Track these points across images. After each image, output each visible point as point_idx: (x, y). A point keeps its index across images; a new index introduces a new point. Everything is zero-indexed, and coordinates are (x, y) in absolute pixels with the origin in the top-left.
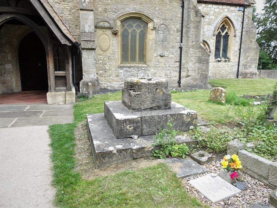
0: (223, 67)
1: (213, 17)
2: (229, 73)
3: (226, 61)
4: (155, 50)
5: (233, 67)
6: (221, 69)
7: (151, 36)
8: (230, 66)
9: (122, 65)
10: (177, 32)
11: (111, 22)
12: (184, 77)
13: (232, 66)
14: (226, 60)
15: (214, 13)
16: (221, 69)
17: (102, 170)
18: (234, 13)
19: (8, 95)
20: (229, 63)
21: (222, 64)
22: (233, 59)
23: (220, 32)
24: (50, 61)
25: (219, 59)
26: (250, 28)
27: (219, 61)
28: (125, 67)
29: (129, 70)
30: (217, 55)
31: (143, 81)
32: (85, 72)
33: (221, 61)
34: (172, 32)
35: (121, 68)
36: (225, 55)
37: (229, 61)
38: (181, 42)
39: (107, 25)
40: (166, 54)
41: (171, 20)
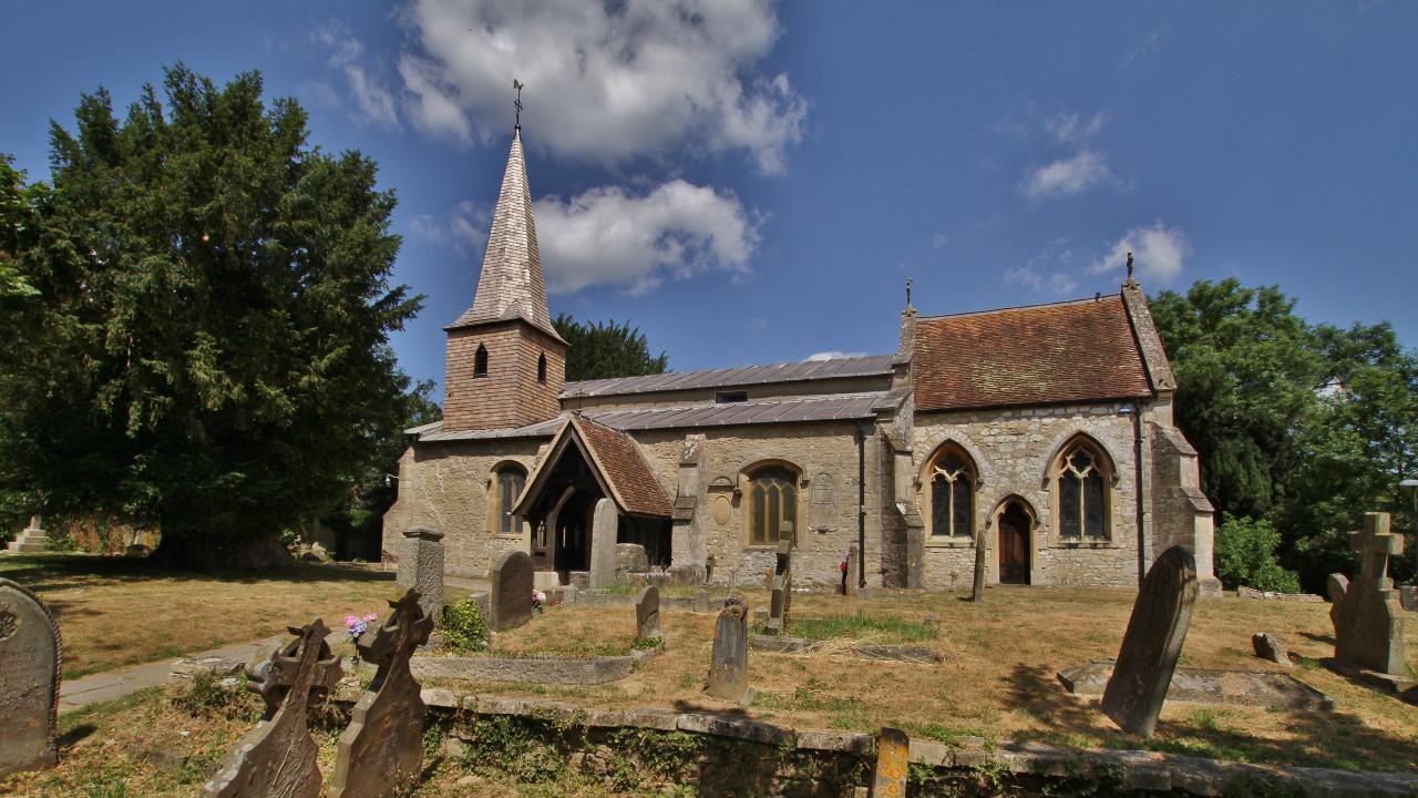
0: (1090, 562)
1: (1040, 438)
2: (1108, 579)
3: (1094, 546)
4: (810, 520)
5: (1126, 563)
6: (1082, 566)
7: (802, 494)
8: (1111, 558)
9: (751, 546)
10: (854, 485)
11: (733, 478)
12: (872, 573)
13: (1117, 559)
14: (1096, 544)
15: (1040, 428)
16: (1082, 566)
17: (462, 500)
18: (1110, 430)
19: (870, 795)
20: (1109, 552)
21: (1084, 555)
22: (1122, 541)
23: (1069, 473)
24: (1291, 664)
25: (1073, 540)
26: (1163, 454)
27: (1071, 546)
28: (756, 550)
29: (761, 555)
30: (1069, 525)
31: (1396, 701)
32: (676, 554)
33: (1077, 544)
34: (843, 486)
35: (747, 551)
36: (1099, 523)
37: (1105, 547)
38: (862, 502)
39: (725, 482)
40: (830, 526)
41: (841, 464)
